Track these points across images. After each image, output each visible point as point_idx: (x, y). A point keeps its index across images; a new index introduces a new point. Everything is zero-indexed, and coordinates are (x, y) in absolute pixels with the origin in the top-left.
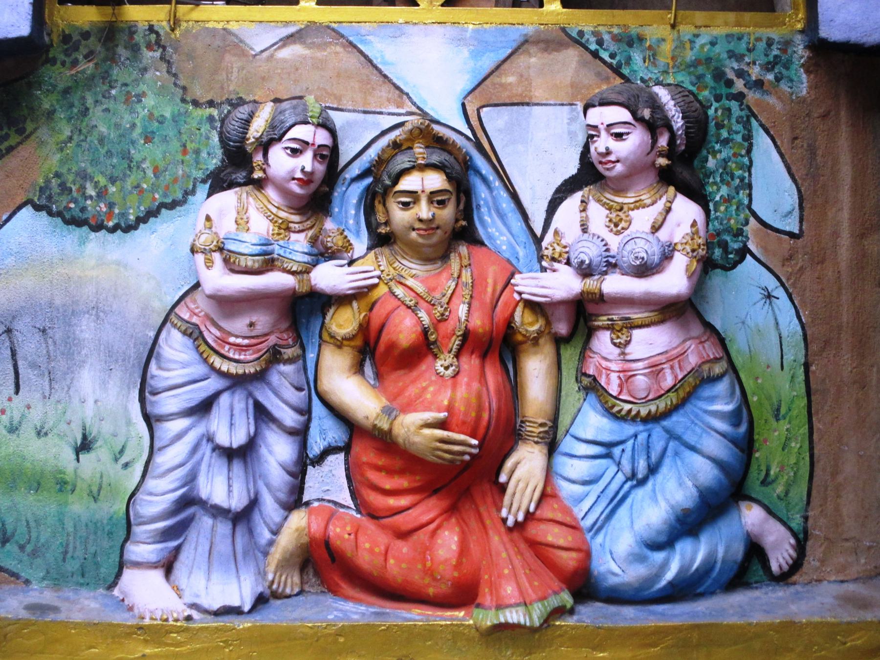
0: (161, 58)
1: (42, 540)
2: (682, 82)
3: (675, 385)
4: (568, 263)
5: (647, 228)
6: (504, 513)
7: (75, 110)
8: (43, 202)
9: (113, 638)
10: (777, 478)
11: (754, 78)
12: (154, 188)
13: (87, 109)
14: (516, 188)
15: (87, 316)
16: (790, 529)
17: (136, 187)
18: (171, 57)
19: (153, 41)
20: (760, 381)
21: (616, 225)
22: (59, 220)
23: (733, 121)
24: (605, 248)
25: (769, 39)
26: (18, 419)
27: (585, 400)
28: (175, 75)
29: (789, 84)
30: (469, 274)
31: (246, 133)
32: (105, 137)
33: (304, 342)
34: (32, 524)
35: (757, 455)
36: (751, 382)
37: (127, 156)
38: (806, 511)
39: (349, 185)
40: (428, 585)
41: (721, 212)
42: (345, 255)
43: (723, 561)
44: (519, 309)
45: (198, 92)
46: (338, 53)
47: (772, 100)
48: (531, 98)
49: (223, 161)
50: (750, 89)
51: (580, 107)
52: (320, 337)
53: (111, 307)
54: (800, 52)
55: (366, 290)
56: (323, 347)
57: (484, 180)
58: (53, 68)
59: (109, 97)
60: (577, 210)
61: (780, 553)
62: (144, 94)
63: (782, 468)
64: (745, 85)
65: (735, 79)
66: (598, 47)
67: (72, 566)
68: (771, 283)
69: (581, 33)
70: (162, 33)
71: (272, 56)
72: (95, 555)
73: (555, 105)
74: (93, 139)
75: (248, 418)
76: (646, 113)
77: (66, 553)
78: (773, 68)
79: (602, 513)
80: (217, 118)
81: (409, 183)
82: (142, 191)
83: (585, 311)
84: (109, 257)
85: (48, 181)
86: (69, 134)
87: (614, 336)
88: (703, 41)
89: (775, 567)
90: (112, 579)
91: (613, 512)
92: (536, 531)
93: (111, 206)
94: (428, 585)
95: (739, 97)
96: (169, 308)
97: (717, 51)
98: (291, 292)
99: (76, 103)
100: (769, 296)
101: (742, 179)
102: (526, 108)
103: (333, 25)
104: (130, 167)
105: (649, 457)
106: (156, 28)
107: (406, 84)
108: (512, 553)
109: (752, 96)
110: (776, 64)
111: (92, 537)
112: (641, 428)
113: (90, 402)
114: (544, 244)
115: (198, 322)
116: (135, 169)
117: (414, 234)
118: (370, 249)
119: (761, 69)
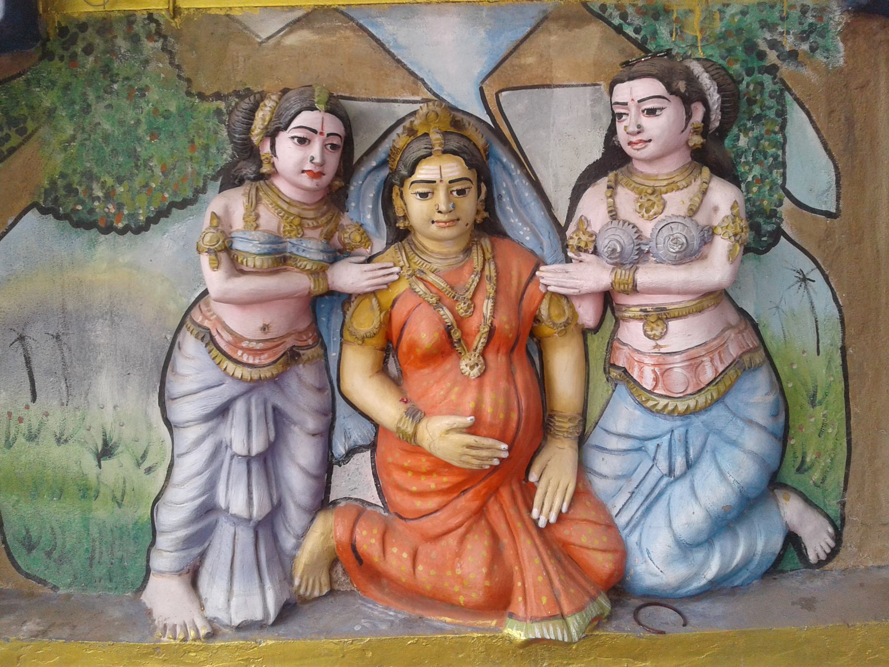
0: (163, 49)
1: (68, 547)
2: (712, 56)
3: (715, 379)
4: (595, 252)
5: (683, 211)
6: (535, 513)
7: (77, 107)
8: (50, 205)
9: (130, 658)
10: (813, 465)
11: (788, 49)
12: (162, 188)
13: (89, 106)
14: (538, 175)
15: (101, 320)
16: (827, 516)
17: (144, 187)
18: (173, 46)
19: (154, 31)
20: (795, 367)
21: (647, 211)
22: (67, 223)
23: (766, 95)
24: (637, 235)
25: (803, 6)
26: (37, 427)
27: (614, 391)
28: (178, 67)
29: (825, 54)
30: (492, 267)
31: (252, 124)
32: (109, 134)
33: (326, 341)
34: (58, 531)
35: (792, 442)
36: (786, 368)
37: (133, 155)
38: (843, 497)
39: (366, 178)
40: (459, 594)
41: (754, 193)
42: (362, 250)
43: (762, 555)
44: (545, 302)
45: (203, 84)
46: (348, 38)
47: (806, 72)
48: (551, 79)
49: (233, 156)
50: (784, 60)
51: (604, 87)
52: (342, 336)
53: (125, 310)
54: (837, 19)
55: (385, 287)
56: (344, 346)
57: (505, 167)
58: (51, 63)
59: (111, 93)
60: (603, 197)
61: (817, 539)
62: (147, 88)
63: (819, 455)
64: (778, 57)
65: (768, 50)
66: (622, 21)
67: (99, 571)
68: (807, 265)
69: (603, 7)
70: (162, 21)
71: (279, 43)
72: (121, 559)
73: (577, 86)
74: (97, 137)
75: (267, 423)
76: (682, 86)
77: (92, 559)
78: (808, 38)
79: (638, 510)
80: (225, 111)
81: (424, 172)
82: (150, 190)
83: (612, 300)
84: (121, 260)
85: (53, 183)
86: (72, 132)
87: (648, 329)
88: (733, 12)
89: (812, 558)
90: (139, 583)
91: (648, 509)
92: (567, 532)
93: (120, 206)
94: (459, 594)
95: (772, 70)
96: (185, 310)
97: (749, 21)
98: (307, 292)
99: (78, 100)
100: (804, 279)
101: (775, 158)
102: (548, 90)
103: (343, 8)
104: (137, 165)
105: (687, 453)
106: (155, 17)
107: (420, 69)
108: (546, 557)
109: (786, 69)
110: (811, 32)
111: (117, 542)
112: (679, 423)
113: (109, 408)
114: (568, 233)
115: (209, 326)
116: (142, 168)
117: (434, 227)
118: (389, 245)
119: (796, 39)
